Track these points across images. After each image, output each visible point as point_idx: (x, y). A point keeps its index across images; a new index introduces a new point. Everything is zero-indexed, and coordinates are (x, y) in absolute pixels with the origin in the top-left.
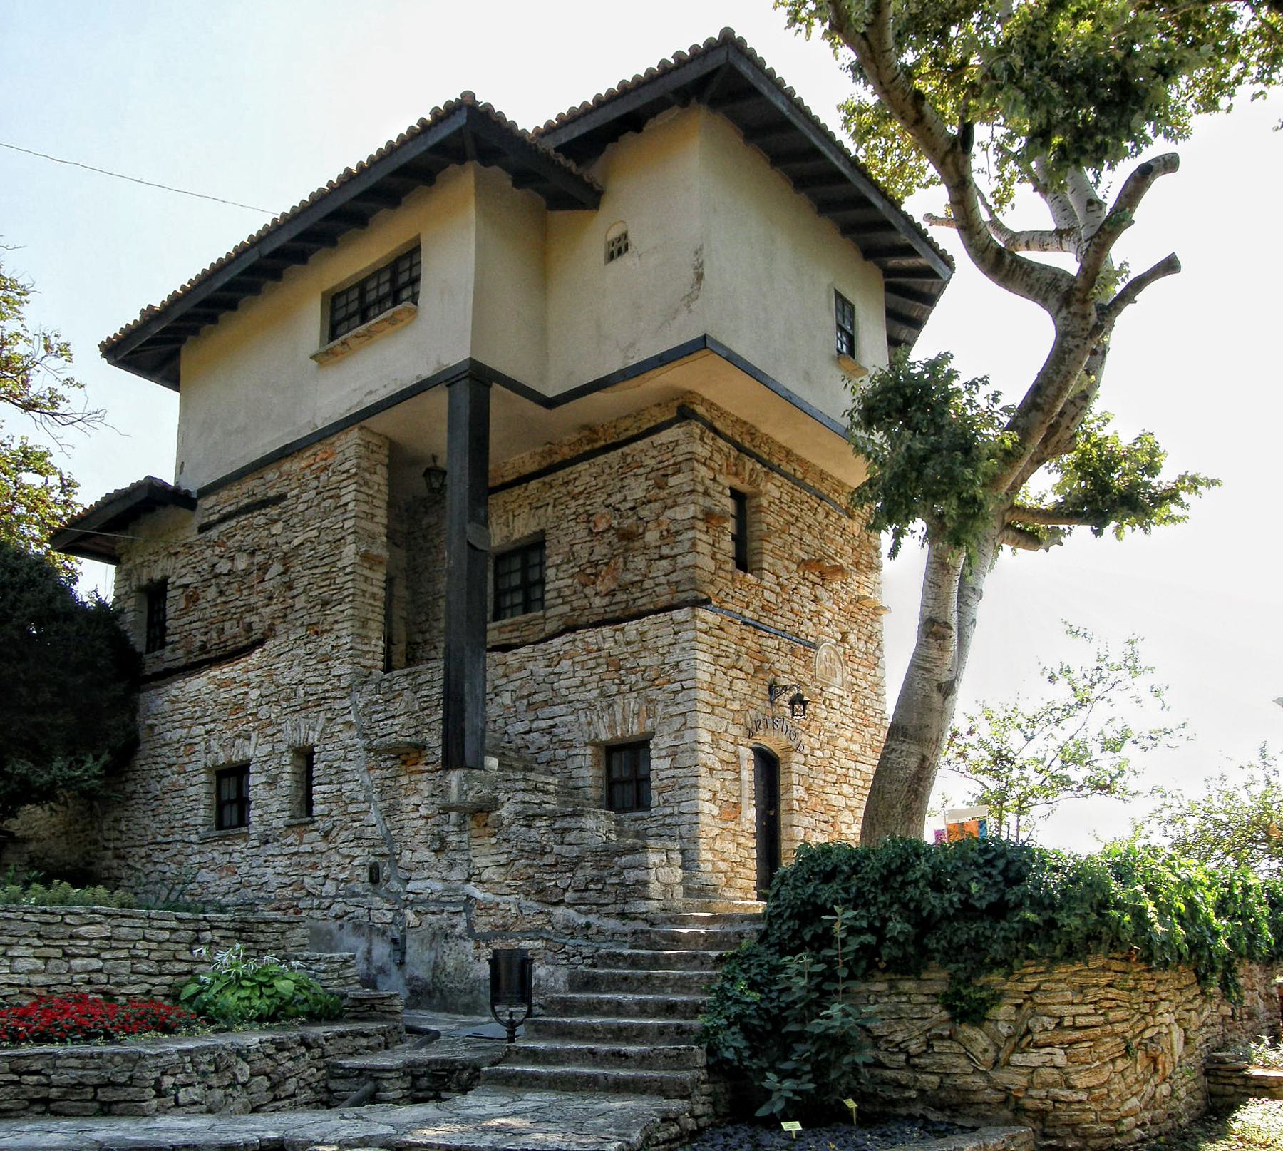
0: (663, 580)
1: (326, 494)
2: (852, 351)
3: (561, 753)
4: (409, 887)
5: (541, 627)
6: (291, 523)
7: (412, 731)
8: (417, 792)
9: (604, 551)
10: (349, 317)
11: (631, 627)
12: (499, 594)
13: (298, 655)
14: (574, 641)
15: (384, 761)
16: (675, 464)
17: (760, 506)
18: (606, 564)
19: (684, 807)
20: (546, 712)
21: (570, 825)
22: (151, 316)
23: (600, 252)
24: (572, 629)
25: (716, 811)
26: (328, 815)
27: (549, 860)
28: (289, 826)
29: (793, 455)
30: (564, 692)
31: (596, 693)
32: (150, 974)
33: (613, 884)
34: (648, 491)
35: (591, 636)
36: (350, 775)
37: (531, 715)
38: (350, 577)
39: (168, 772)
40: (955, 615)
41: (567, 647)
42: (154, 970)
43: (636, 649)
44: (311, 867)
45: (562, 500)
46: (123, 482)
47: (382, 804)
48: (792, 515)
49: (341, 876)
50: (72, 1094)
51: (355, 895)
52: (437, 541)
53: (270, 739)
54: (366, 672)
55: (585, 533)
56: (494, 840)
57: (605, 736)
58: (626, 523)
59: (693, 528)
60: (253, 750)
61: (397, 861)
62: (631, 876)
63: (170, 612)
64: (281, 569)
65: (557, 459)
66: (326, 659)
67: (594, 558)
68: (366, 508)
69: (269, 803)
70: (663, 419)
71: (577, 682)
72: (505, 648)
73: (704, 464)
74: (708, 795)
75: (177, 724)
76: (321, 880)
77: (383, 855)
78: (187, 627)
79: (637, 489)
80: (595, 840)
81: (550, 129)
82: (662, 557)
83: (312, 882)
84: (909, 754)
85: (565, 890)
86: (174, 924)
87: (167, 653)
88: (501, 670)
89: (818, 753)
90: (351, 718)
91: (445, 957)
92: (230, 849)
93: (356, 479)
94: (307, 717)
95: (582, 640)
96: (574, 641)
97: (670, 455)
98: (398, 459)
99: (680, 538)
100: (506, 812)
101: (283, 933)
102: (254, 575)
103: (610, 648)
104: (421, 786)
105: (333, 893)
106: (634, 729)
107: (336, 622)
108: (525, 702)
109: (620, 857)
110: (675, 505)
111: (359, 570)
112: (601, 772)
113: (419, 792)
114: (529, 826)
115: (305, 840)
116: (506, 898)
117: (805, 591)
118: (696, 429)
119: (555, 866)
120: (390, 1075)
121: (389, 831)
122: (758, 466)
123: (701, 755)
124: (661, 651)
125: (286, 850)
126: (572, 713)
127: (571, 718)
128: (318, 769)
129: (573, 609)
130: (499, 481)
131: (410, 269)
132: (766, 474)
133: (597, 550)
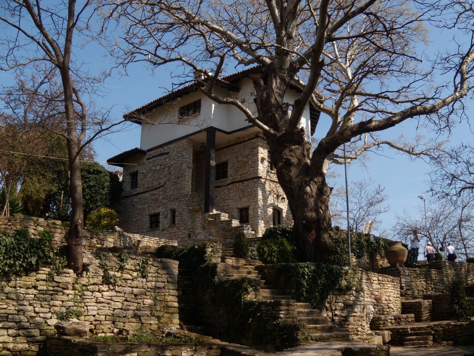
8: (199, 218)
19: (256, 221)
20: (228, 201)
27: (226, 230)
55: (236, 161)
57: (240, 206)
58: (245, 159)
63: (139, 179)
66: (179, 189)
71: (234, 195)
87: (138, 189)
88: (218, 192)
90: (184, 202)
106: (246, 205)
118: (259, 139)
128: (177, 214)
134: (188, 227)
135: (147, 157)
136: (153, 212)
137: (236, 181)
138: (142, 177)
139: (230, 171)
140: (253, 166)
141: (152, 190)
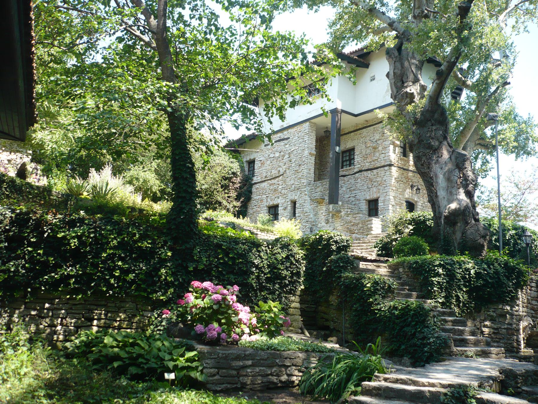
3: (357, 202)
11: (375, 171)
12: (343, 162)
20: (354, 192)
23: (369, 80)
24: (361, 171)
27: (352, 224)
31: (366, 187)
57: (368, 198)
62: (369, 226)
68: (310, 141)
72: (344, 176)
79: (377, 136)
88: (343, 181)
98: (317, 128)
112: (367, 207)
113: (323, 210)
130: (343, 133)
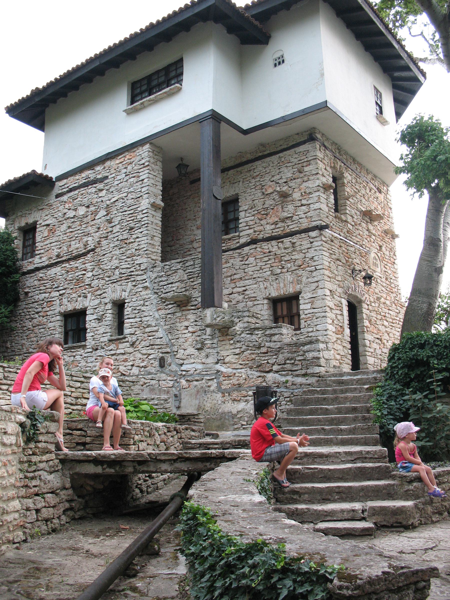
0: (304, 216)
1: (131, 176)
2: (381, 112)
4: (183, 368)
5: (237, 241)
6: (111, 190)
7: (184, 290)
8: (187, 320)
9: (271, 203)
10: (141, 93)
13: (116, 255)
14: (256, 248)
15: (166, 305)
16: (307, 161)
17: (344, 183)
18: (272, 209)
20: (242, 283)
21: (275, 332)
22: (36, 93)
25: (334, 330)
26: (133, 334)
27: (264, 350)
28: (110, 341)
29: (356, 161)
30: (251, 273)
31: (269, 273)
32: (72, 404)
33: (300, 360)
34: (293, 174)
35: (266, 246)
36: (147, 311)
37: (233, 285)
38: (146, 215)
39: (37, 316)
40: (442, 235)
41: (252, 251)
42: (74, 402)
43: (290, 251)
44: (123, 361)
45: (248, 179)
46: (19, 174)
47: (166, 327)
48: (357, 189)
49: (142, 365)
50: (96, 440)
51: (150, 373)
52: (178, 201)
53: (98, 297)
54: (153, 262)
55: (260, 194)
56: (232, 342)
57: (274, 294)
58: (284, 189)
59: (318, 191)
60: (89, 303)
61: (175, 355)
62: (310, 355)
63: (38, 239)
64: (105, 213)
65: (244, 160)
67: (266, 206)
68: (153, 181)
69: (98, 329)
70: (301, 140)
73: (321, 161)
74: (330, 321)
75: (42, 291)
76: (130, 367)
77: (167, 353)
78: (49, 245)
80: (287, 340)
81: (247, 7)
82: (302, 205)
83: (124, 368)
84: (423, 302)
85: (273, 364)
86: (82, 379)
87: (37, 260)
89: (373, 304)
91: (205, 402)
92: (74, 354)
93: (148, 167)
94: (121, 285)
95: (260, 247)
96: (256, 248)
97: (305, 157)
99: (311, 196)
100: (238, 327)
101: (130, 387)
102: (89, 217)
103: (275, 251)
104: (189, 317)
105: (137, 373)
106: (291, 290)
107: (138, 238)
108: (229, 279)
109: (304, 346)
110: (309, 180)
111: (150, 211)
114: (251, 334)
115: (120, 347)
116: (239, 370)
117: (364, 225)
119: (267, 353)
120: (216, 446)
121: (170, 340)
122: (343, 165)
123: (327, 302)
124: (303, 251)
125: (109, 353)
126: (256, 283)
127: (255, 286)
128: (127, 311)
129: (255, 232)
131: (176, 70)
132: (346, 169)
133: (267, 203)
134: (158, 342)
135: (57, 190)
136: (70, 307)
137: (260, 237)
138: (46, 234)
139: (245, 217)
140: (304, 202)
141: (68, 260)
